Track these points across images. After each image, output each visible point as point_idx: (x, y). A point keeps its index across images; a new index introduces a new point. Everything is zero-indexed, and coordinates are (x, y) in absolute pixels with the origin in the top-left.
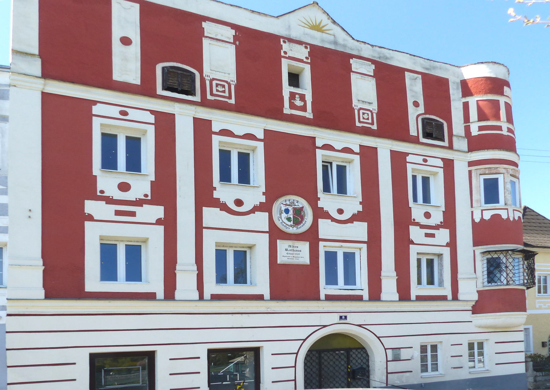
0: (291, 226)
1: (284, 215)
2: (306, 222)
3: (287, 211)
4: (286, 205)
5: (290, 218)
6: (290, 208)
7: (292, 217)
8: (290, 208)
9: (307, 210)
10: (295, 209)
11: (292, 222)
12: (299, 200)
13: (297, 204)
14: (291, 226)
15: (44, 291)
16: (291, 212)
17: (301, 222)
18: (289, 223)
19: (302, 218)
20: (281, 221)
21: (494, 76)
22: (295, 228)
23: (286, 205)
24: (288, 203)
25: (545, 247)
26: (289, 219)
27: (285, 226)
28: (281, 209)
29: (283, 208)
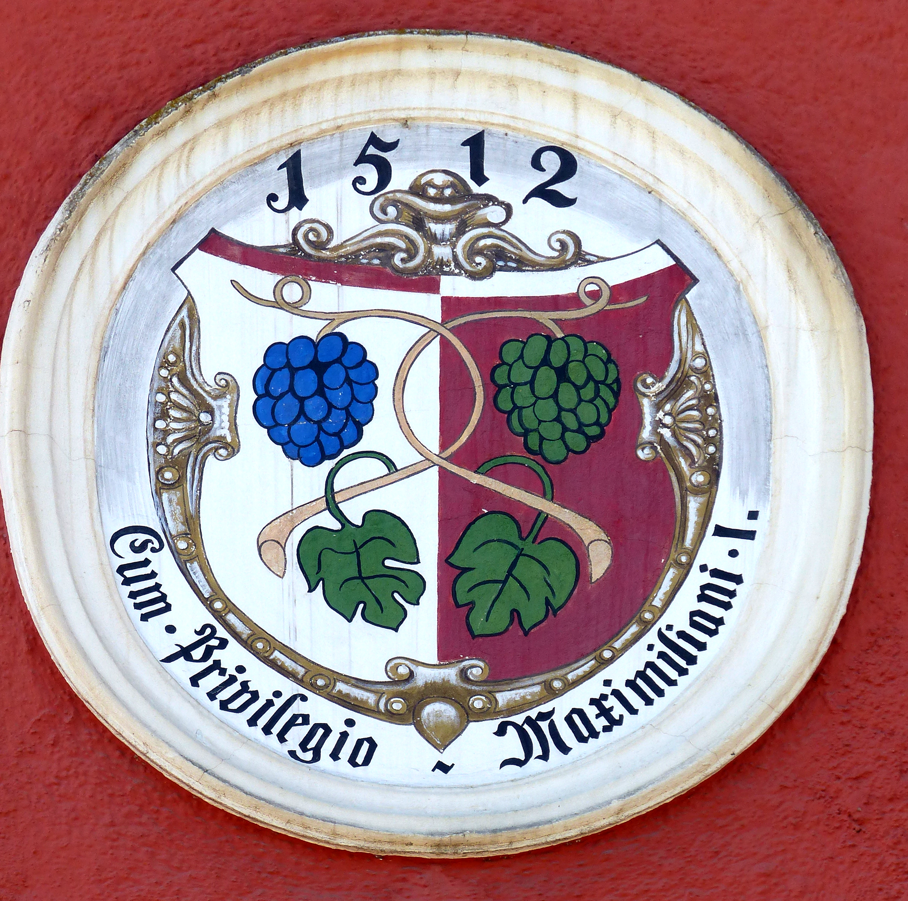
0: (404, 699)
1: (257, 487)
2: (721, 589)
3: (313, 400)
4: (301, 261)
5: (387, 530)
6: (394, 333)
7: (418, 505)
8: (394, 333)
9: (750, 332)
10: (484, 344)
11: (423, 620)
12: (590, 137)
13: (535, 226)
14: (404, 699)
15: (557, 168)
16: (408, 416)
17: (622, 603)
18: (361, 650)
19: (651, 516)
20: (189, 615)
21: (287, 192)
22: (481, 747)
23: (301, 261)
24: (343, 211)
25: (418, 473)
26: (353, 565)
27: (274, 719)
28: (177, 366)
29: (240, 331)
